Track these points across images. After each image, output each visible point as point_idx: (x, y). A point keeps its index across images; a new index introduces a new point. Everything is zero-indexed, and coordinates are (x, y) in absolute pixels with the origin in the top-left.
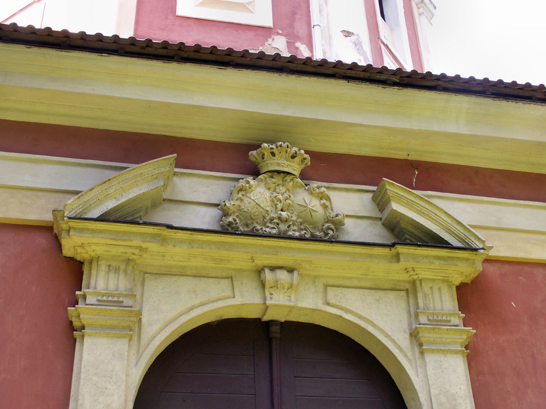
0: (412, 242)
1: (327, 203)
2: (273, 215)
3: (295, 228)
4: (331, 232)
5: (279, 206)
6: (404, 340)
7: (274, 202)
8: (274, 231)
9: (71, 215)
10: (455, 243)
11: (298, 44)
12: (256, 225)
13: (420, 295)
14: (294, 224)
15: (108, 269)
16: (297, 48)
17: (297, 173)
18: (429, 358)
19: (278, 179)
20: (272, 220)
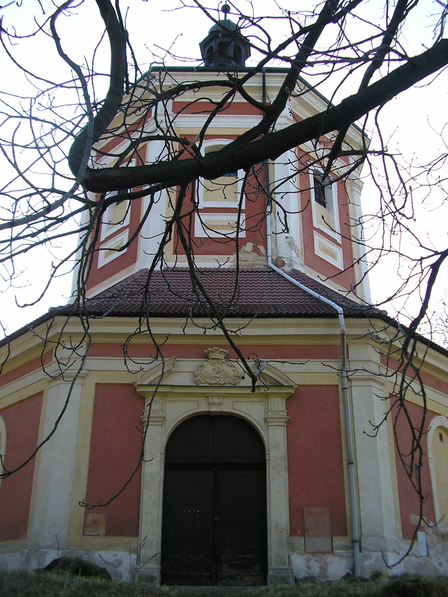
0: (275, 384)
1: (234, 369)
2: (213, 376)
3: (222, 380)
4: (236, 381)
5: (216, 372)
6: (262, 423)
7: (214, 370)
8: (214, 382)
9: (111, 246)
10: (285, 384)
11: (259, 246)
12: (207, 380)
13: (269, 404)
14: (222, 379)
15: (357, 251)
16: (259, 249)
17: (223, 358)
18: (270, 428)
19: (214, 361)
20: (213, 377)
